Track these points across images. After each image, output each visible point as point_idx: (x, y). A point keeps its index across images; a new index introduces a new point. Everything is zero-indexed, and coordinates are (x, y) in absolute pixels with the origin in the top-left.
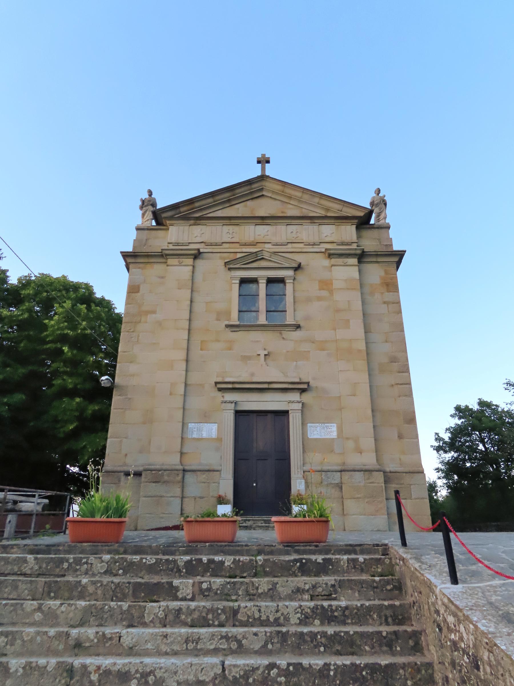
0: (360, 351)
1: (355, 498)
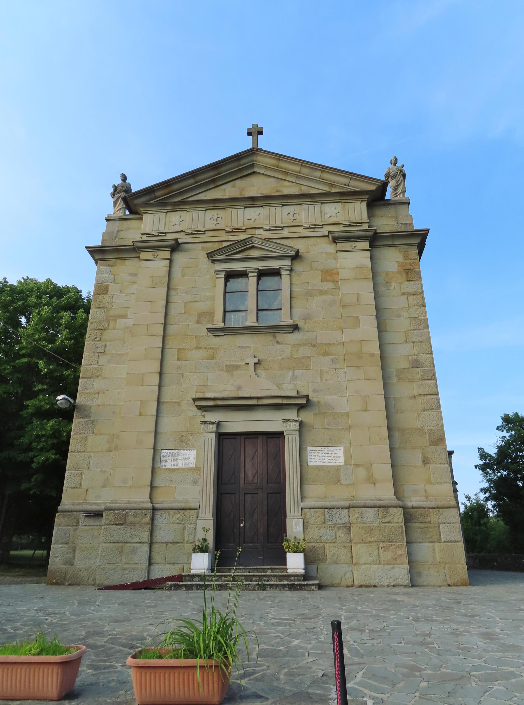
0: (372, 355)
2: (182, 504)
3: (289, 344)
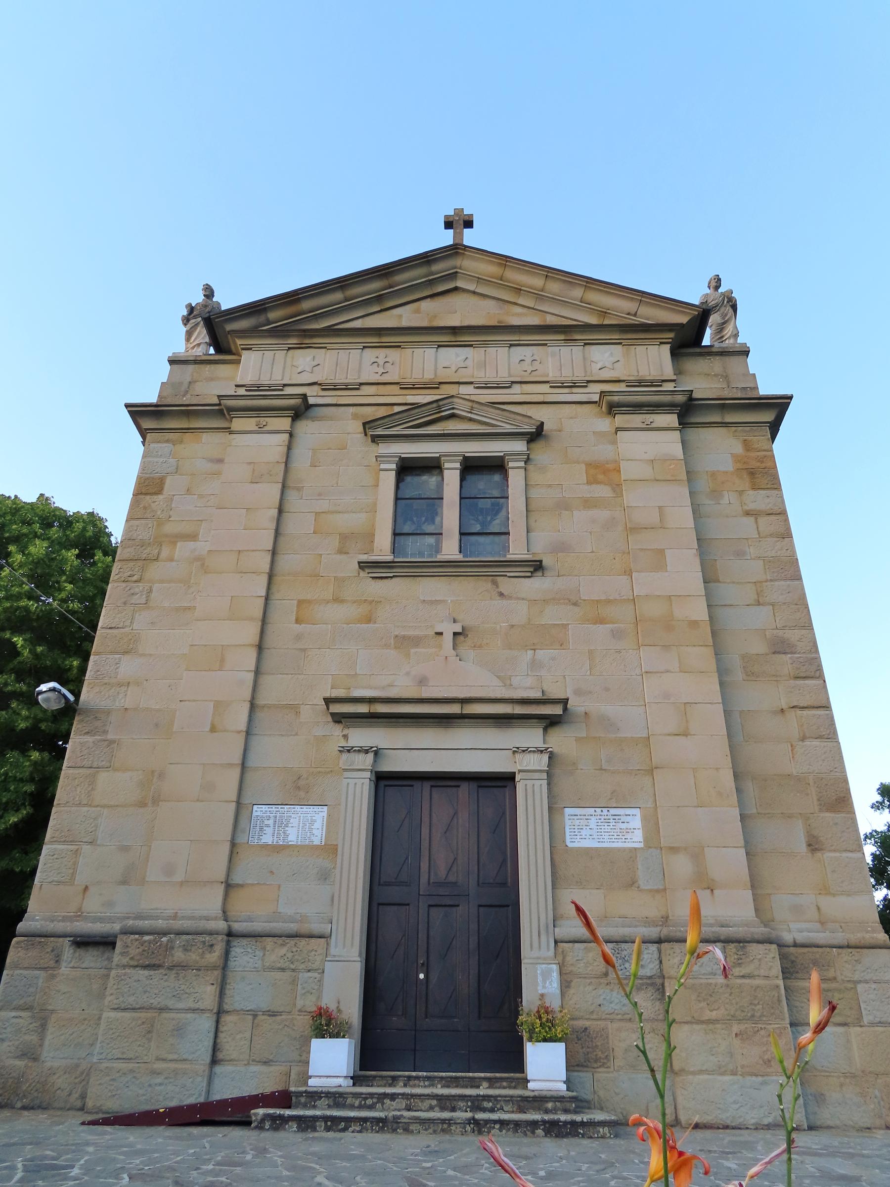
0: (694, 624)
1: (703, 1022)
2: (292, 925)
3: (523, 599)
